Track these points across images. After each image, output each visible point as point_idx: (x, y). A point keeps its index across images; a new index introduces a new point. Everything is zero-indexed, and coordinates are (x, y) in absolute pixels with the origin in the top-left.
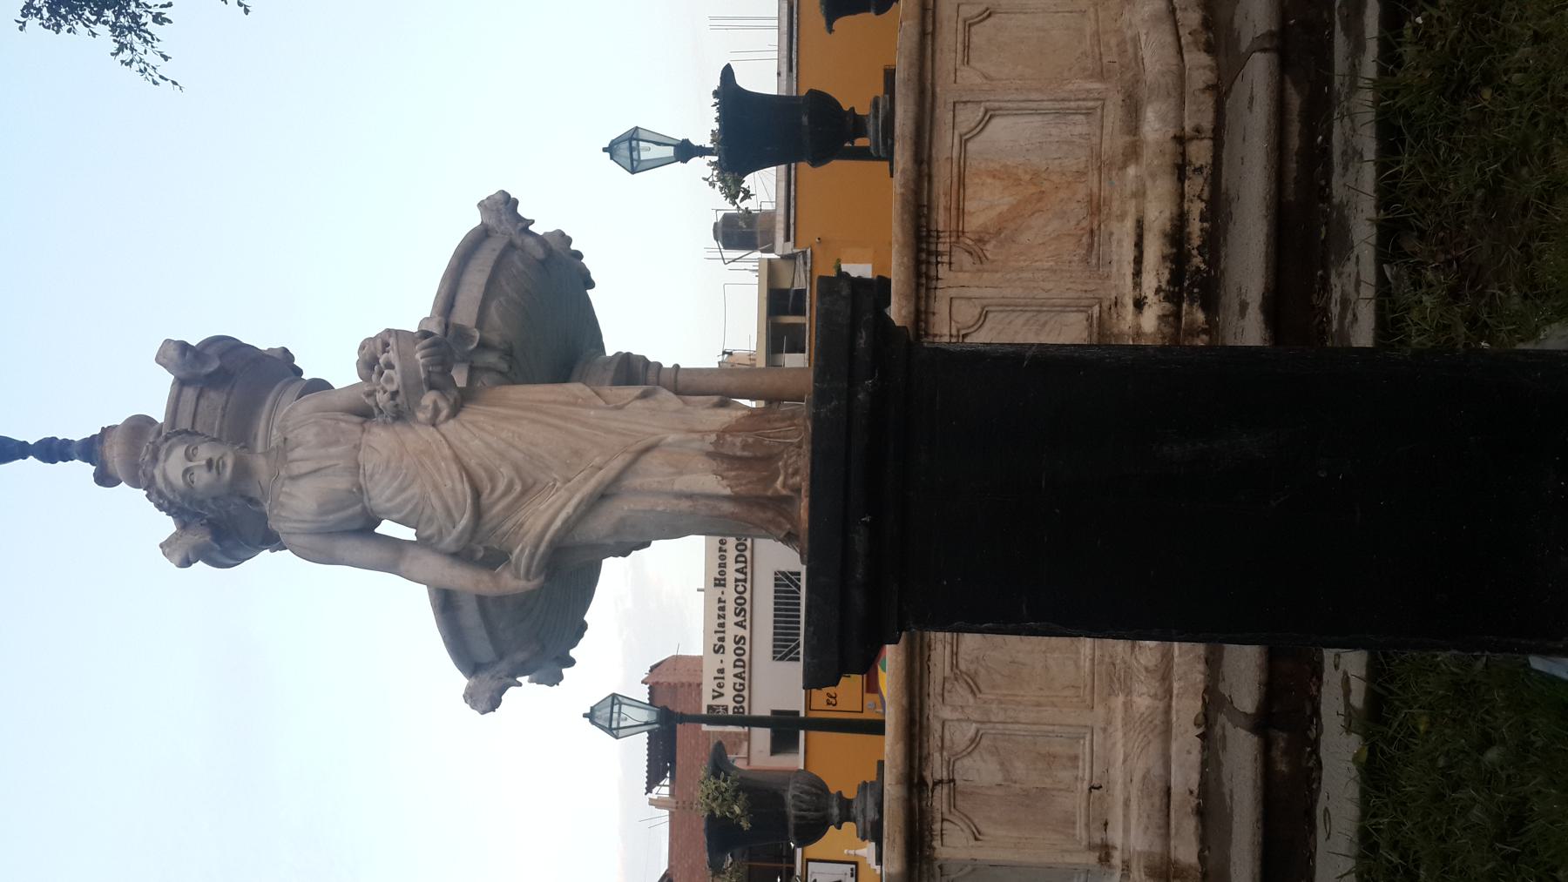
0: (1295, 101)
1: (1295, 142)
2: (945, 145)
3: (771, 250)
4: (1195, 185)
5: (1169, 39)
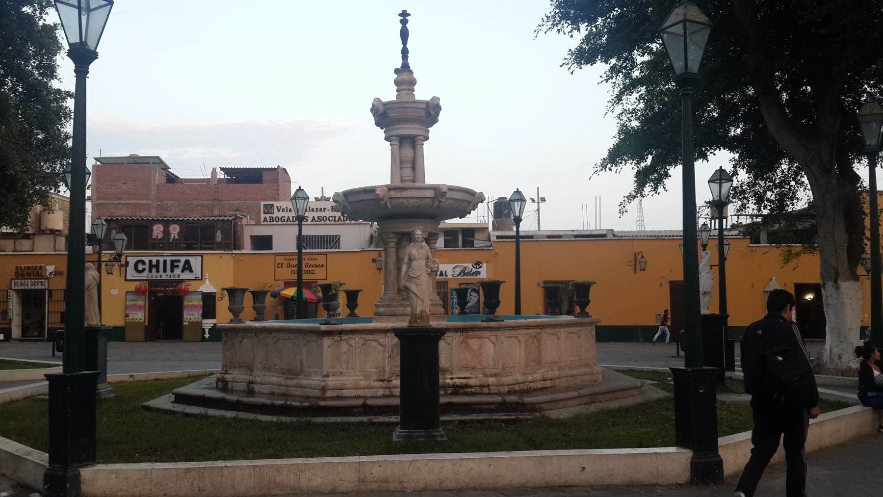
0: (493, 406)
1: (484, 407)
2: (487, 334)
3: (494, 228)
4: (478, 389)
5: (511, 382)
